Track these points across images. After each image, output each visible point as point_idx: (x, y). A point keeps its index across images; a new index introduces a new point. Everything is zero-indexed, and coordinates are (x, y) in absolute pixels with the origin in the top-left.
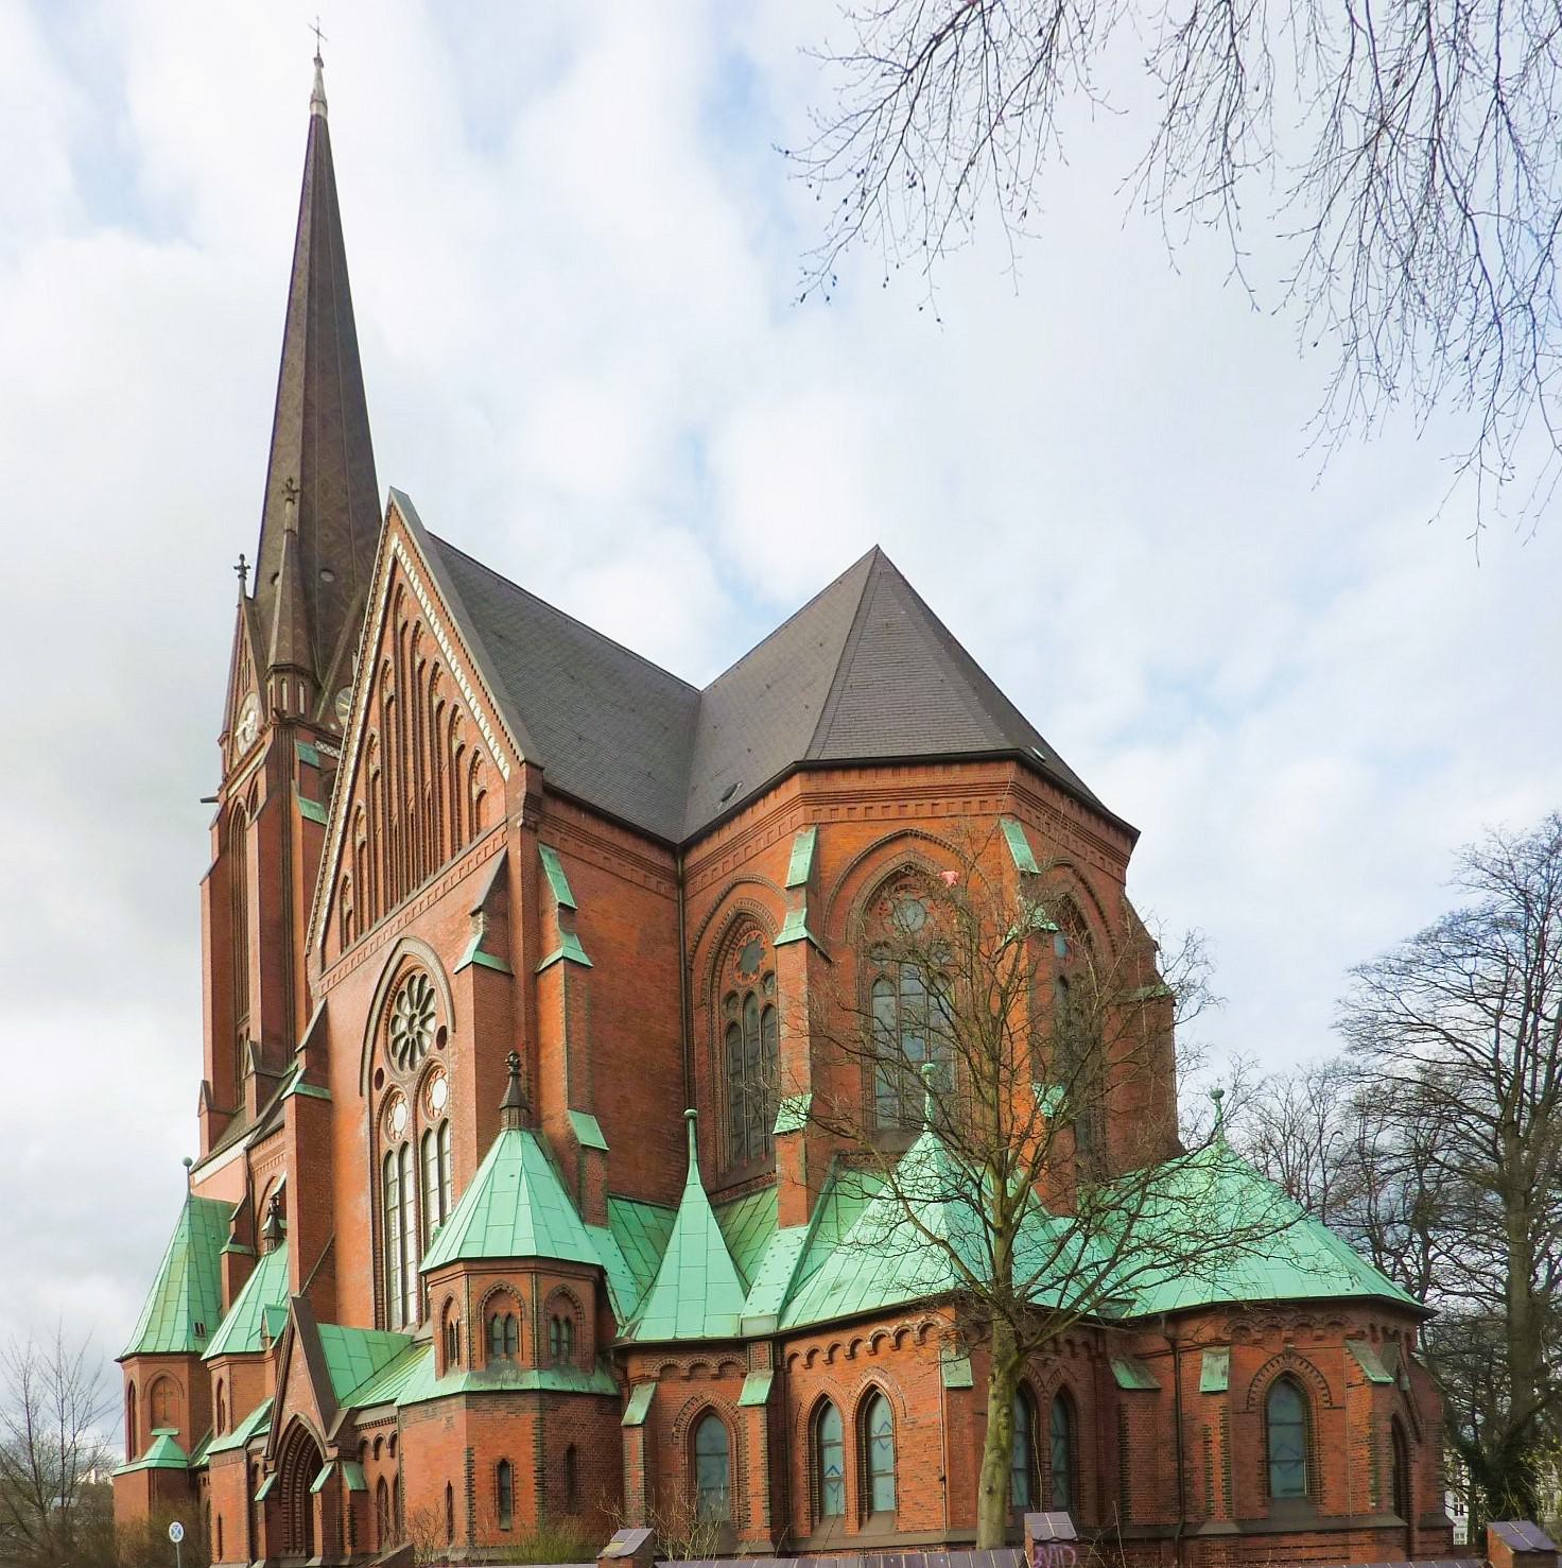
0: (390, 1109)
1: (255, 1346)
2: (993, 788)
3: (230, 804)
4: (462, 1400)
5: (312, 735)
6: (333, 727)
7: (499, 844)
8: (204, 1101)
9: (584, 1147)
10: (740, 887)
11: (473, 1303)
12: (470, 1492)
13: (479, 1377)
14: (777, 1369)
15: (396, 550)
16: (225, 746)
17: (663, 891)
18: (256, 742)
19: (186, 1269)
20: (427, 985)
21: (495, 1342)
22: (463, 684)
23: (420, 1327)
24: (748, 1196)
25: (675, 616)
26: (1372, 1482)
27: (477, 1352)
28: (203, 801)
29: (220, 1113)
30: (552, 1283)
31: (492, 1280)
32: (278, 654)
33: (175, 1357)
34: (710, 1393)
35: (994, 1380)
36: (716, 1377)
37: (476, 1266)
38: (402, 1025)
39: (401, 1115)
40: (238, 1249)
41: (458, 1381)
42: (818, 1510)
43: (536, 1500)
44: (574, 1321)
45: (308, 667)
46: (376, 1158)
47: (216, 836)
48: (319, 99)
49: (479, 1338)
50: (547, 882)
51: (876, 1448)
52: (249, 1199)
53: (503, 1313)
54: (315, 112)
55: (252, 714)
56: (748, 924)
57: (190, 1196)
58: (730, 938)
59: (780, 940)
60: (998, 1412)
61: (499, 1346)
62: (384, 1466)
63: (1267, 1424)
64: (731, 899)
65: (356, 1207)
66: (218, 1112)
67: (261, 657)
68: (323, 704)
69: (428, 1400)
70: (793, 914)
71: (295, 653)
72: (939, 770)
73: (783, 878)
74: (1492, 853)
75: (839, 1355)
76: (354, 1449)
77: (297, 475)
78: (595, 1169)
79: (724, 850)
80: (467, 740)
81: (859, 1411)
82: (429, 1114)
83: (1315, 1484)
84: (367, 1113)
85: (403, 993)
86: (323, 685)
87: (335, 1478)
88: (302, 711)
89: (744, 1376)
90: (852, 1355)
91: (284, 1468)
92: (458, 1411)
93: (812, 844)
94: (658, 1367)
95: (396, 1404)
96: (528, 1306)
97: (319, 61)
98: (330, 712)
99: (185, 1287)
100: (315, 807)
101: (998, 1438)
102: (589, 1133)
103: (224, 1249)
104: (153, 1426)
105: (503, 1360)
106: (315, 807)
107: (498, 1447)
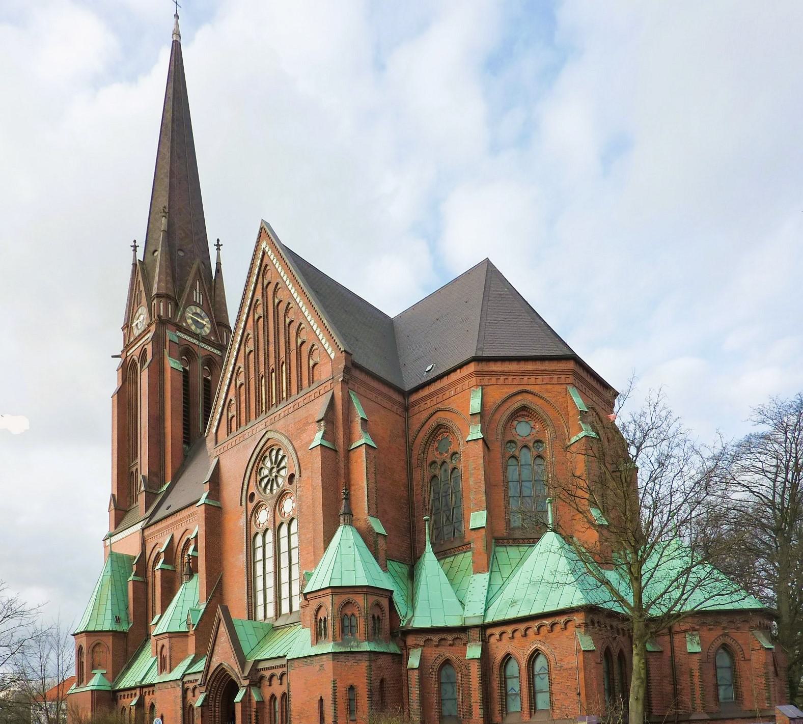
0: (257, 512)
1: (184, 628)
2: (563, 372)
3: (128, 359)
4: (330, 656)
5: (175, 328)
6: (184, 324)
7: (328, 388)
8: (112, 504)
9: (377, 533)
10: (439, 413)
11: (336, 607)
12: (335, 702)
13: (339, 645)
14: (483, 641)
15: (264, 249)
16: (125, 331)
17: (398, 413)
18: (145, 330)
19: (110, 588)
20: (281, 453)
21: (346, 627)
22: (306, 314)
23: (276, 620)
24: (446, 558)
25: (390, 286)
26: (767, 694)
27: (337, 633)
28: (113, 357)
29: (121, 510)
30: (373, 599)
31: (345, 597)
32: (158, 289)
33: (105, 633)
34: (447, 652)
35: (636, 646)
36: (451, 645)
37: (337, 590)
38: (265, 472)
39: (264, 516)
40: (137, 578)
41: (328, 647)
42: (505, 709)
43: (368, 705)
44: (381, 617)
45: (173, 295)
46: (249, 536)
47: (121, 375)
48: (177, 33)
49: (338, 626)
50: (354, 407)
51: (537, 680)
52: (143, 553)
53: (349, 613)
54: (175, 39)
55: (142, 318)
56: (443, 430)
57: (111, 552)
58: (433, 436)
59: (469, 438)
60: (640, 661)
61: (347, 630)
62: (277, 689)
63: (716, 668)
64: (434, 417)
65: (236, 561)
66: (120, 510)
67: (148, 290)
68: (180, 314)
69: (308, 656)
70: (474, 426)
71: (167, 288)
72: (538, 363)
73: (468, 410)
74: (770, 409)
75: (518, 634)
76: (256, 680)
77: (166, 204)
78: (382, 543)
79: (432, 395)
80: (308, 339)
81: (529, 662)
82: (282, 515)
83: (738, 696)
84: (245, 514)
85: (266, 457)
86: (180, 304)
87: (247, 696)
88: (170, 316)
89: (465, 645)
90: (525, 635)
91: (211, 690)
92: (328, 664)
93: (480, 395)
94: (423, 640)
95: (286, 658)
96: (363, 610)
97: (177, 16)
98: (183, 318)
99: (110, 598)
100: (176, 362)
101: (639, 673)
102: (379, 528)
103: (131, 578)
104: (93, 668)
105: (350, 637)
106: (176, 362)
107: (349, 679)
